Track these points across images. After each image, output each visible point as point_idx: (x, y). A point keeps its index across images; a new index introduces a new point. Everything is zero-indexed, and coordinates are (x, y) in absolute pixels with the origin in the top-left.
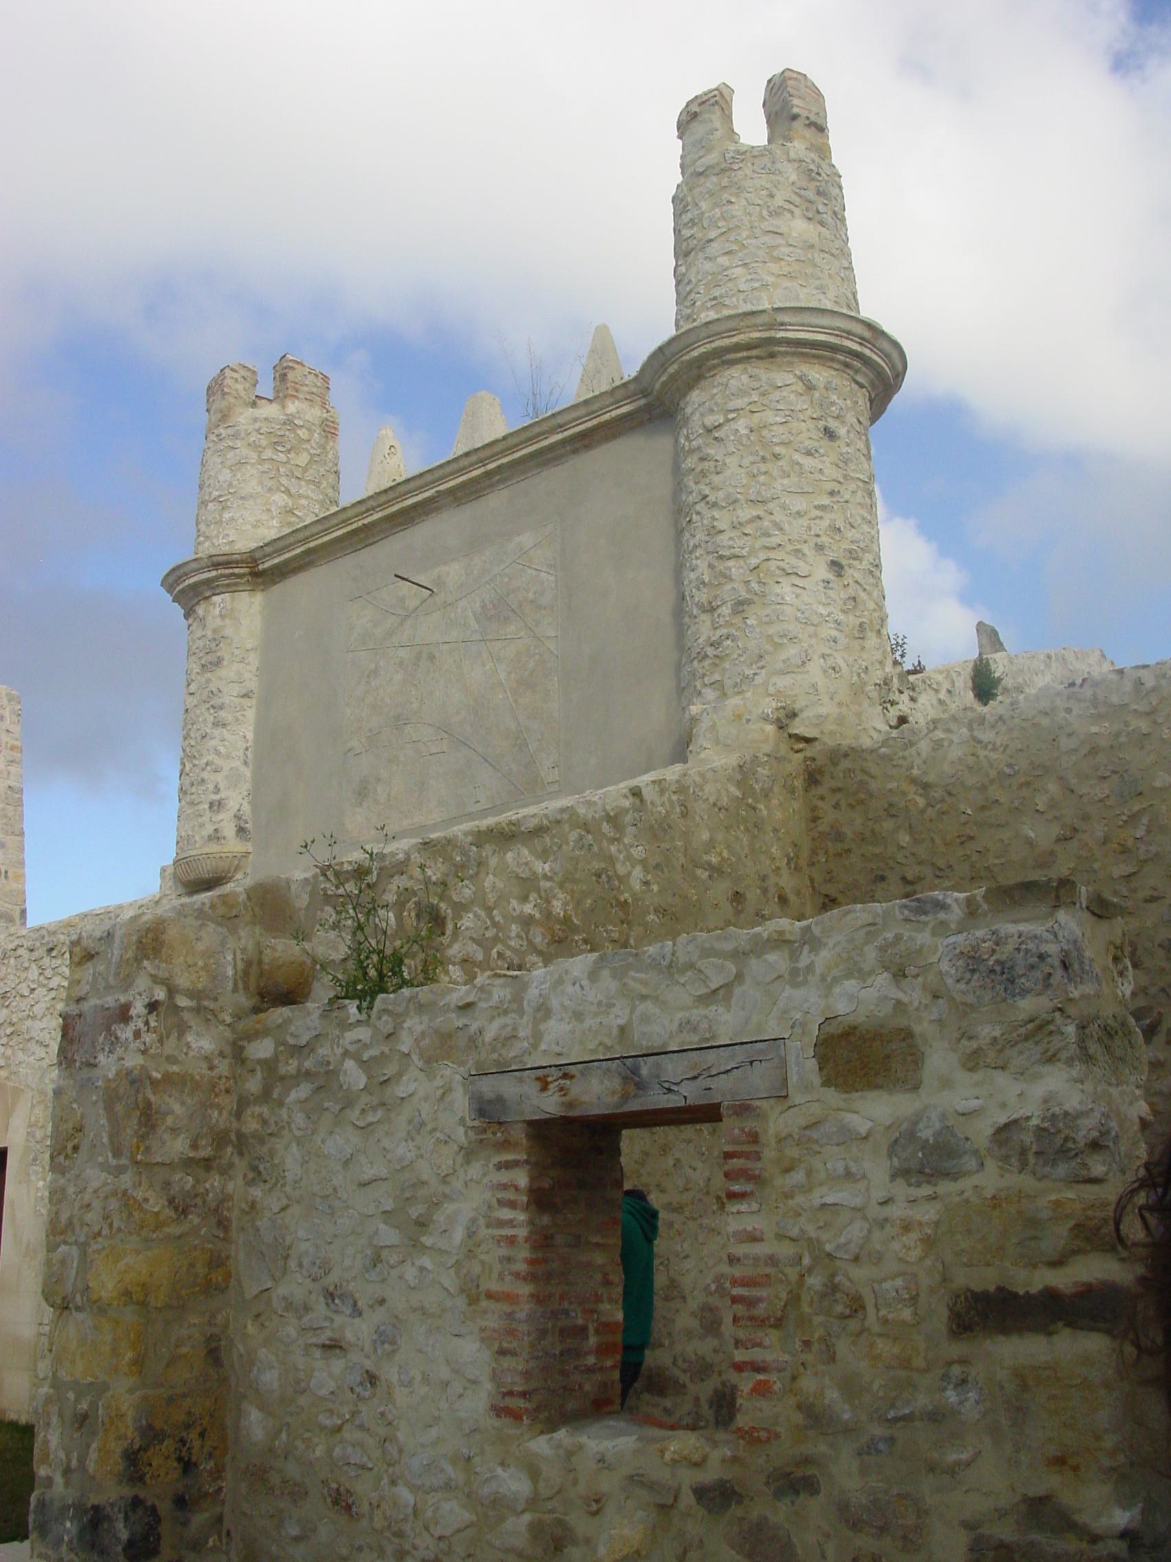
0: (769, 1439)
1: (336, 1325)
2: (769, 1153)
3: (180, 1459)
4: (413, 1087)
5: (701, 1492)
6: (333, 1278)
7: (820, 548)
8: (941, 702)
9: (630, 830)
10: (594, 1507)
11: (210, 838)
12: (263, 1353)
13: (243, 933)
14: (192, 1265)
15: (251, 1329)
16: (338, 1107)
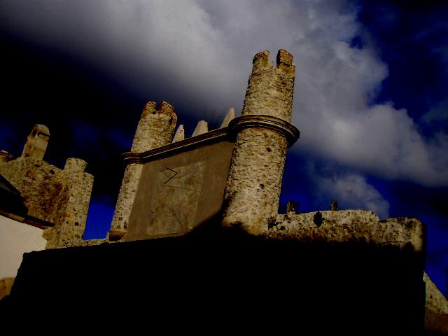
7: (258, 180)
8: (300, 224)
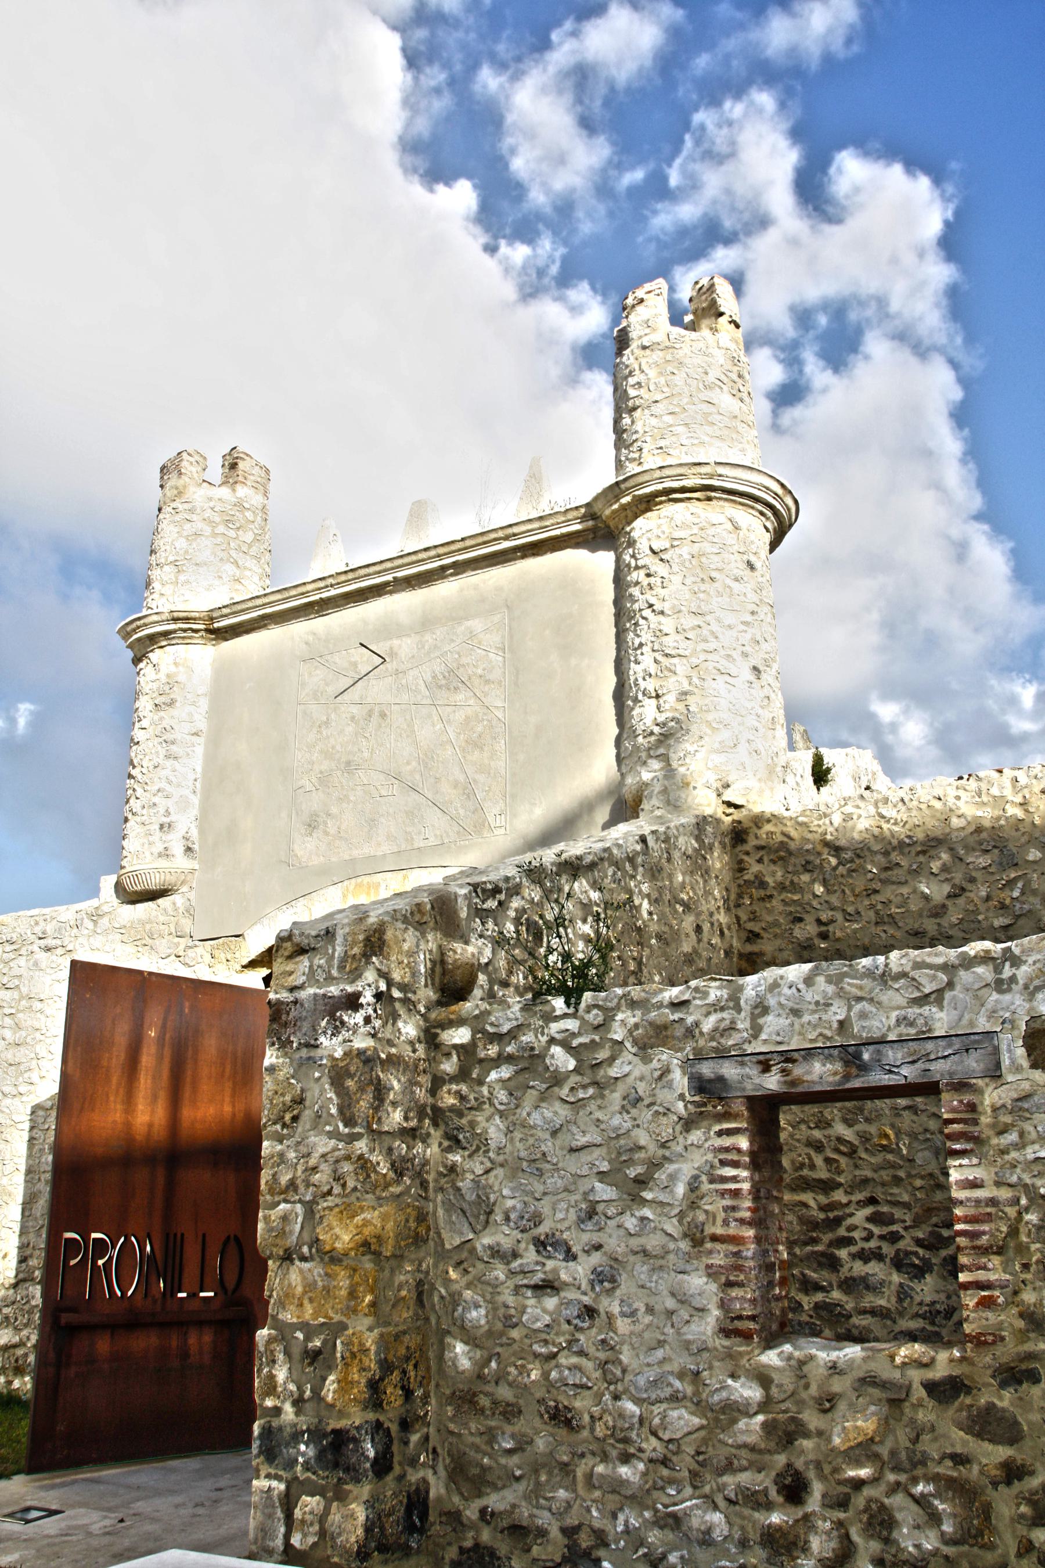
0: (994, 1342)
1: (548, 1268)
2: (985, 1120)
3: (403, 1388)
4: (627, 1069)
5: (931, 1387)
6: (542, 1230)
7: (745, 655)
9: (641, 869)
10: (828, 1405)
11: (160, 855)
12: (468, 1294)
13: (430, 937)
14: (407, 1221)
15: (453, 1274)
16: (545, 1086)
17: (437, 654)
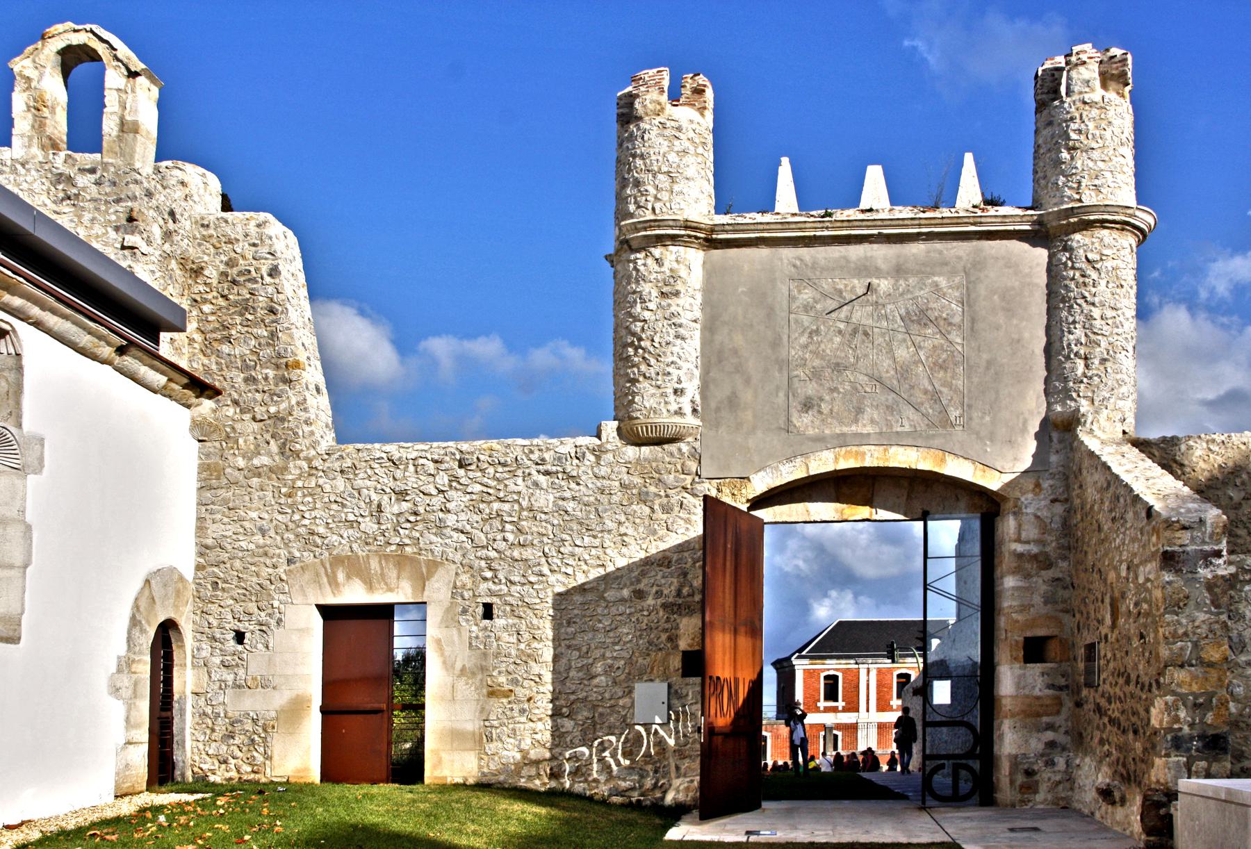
11: (676, 413)
12: (1235, 681)
17: (910, 296)
